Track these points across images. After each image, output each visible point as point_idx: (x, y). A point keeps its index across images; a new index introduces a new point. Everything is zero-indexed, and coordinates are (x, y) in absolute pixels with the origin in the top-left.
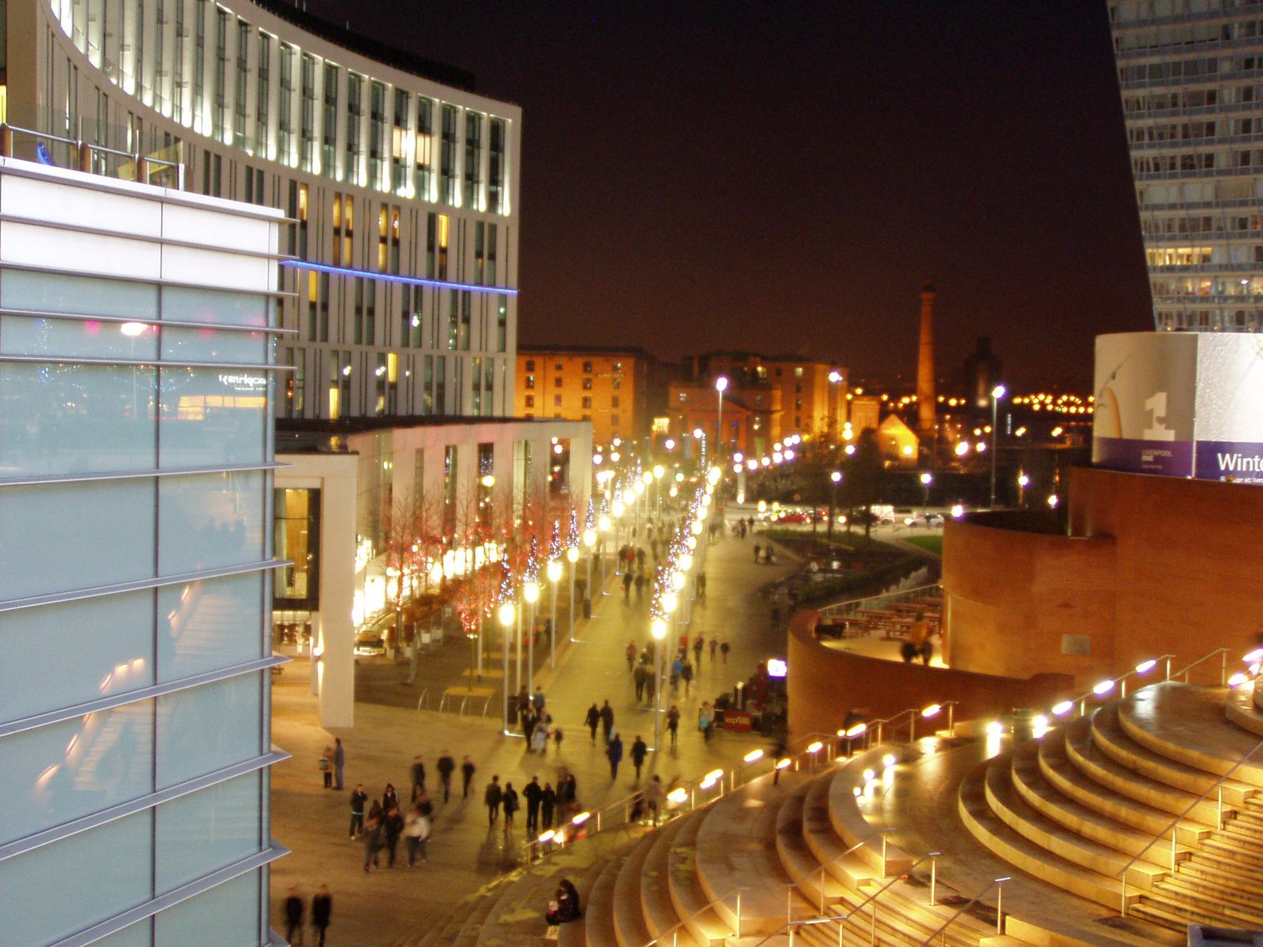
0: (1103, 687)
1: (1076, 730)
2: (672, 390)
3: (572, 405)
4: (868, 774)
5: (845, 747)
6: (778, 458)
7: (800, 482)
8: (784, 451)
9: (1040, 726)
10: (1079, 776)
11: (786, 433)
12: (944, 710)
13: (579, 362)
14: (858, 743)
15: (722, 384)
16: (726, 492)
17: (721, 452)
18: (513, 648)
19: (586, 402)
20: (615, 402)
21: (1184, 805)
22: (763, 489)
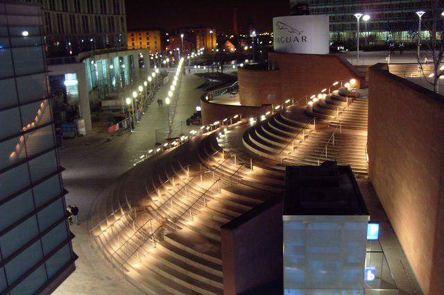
0: (278, 107)
1: (270, 119)
2: (97, 234)
3: (144, 44)
4: (220, 134)
5: (214, 128)
6: (199, 54)
7: (205, 60)
8: (200, 52)
9: (263, 118)
10: (271, 130)
11: (200, 48)
12: (239, 116)
13: (145, 33)
14: (218, 126)
15: (182, 36)
16: (186, 64)
17: (184, 54)
18: (131, 108)
19: (148, 43)
20: (156, 43)
21: (284, 146)
22: (196, 62)
